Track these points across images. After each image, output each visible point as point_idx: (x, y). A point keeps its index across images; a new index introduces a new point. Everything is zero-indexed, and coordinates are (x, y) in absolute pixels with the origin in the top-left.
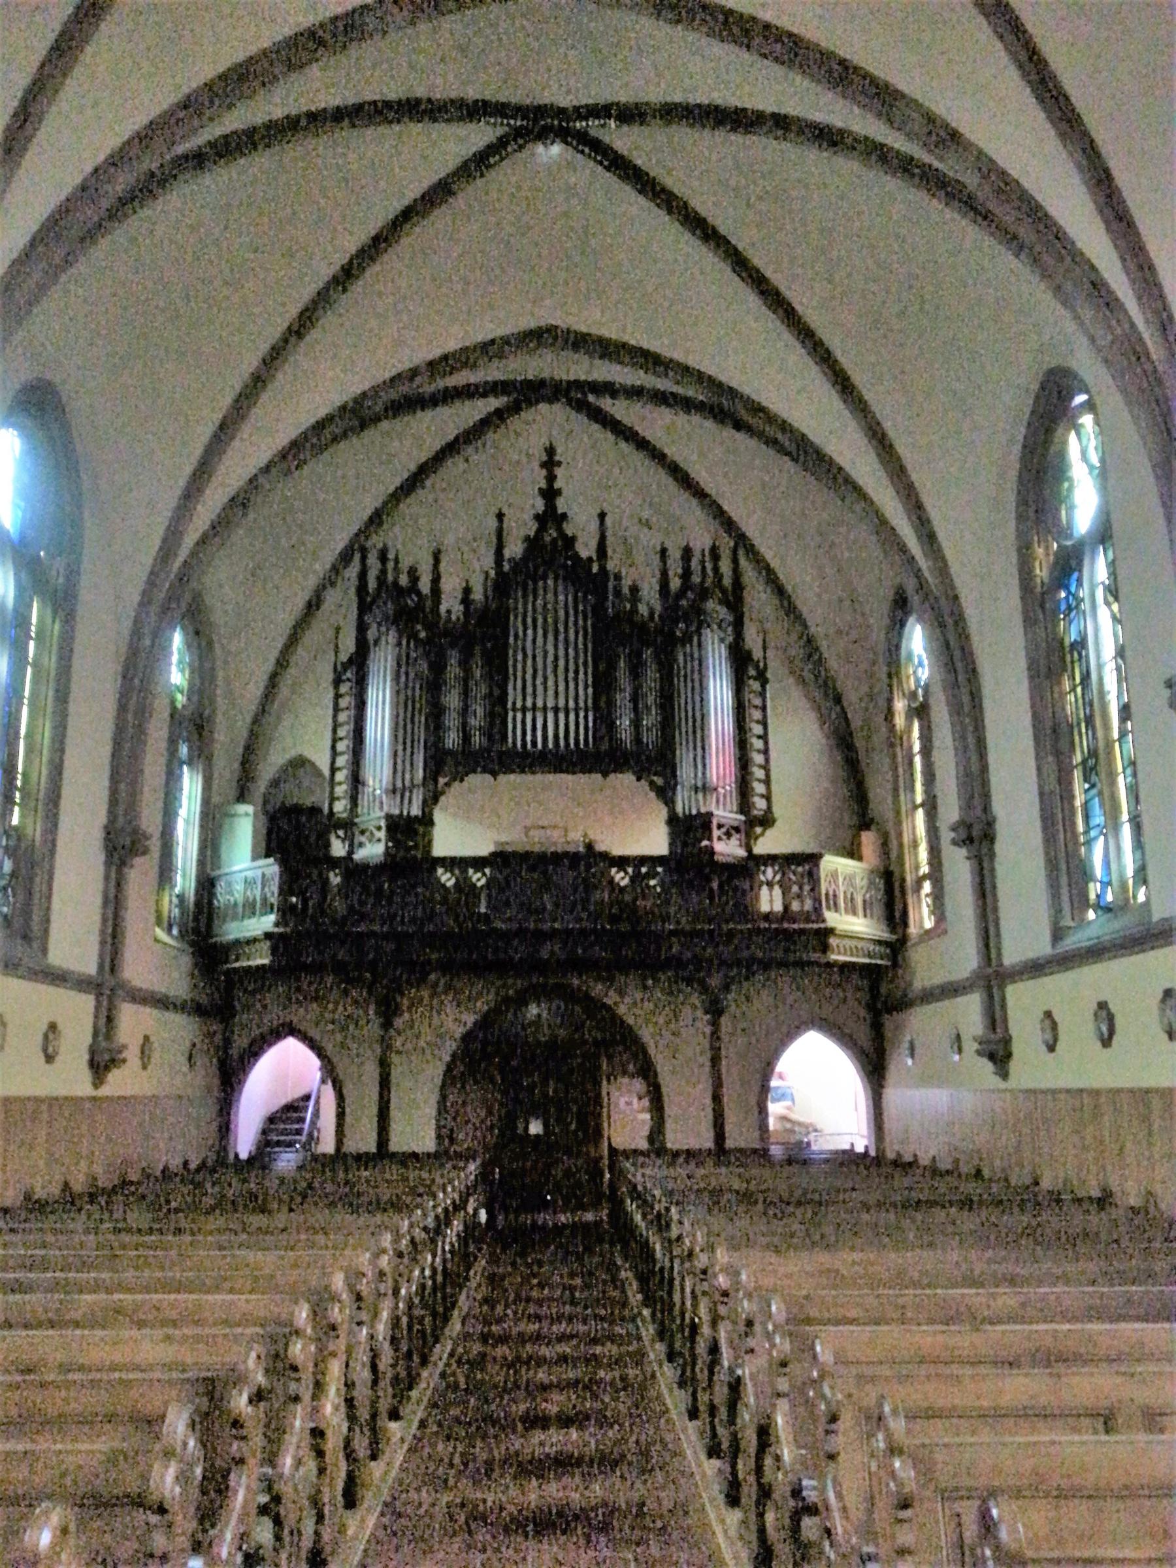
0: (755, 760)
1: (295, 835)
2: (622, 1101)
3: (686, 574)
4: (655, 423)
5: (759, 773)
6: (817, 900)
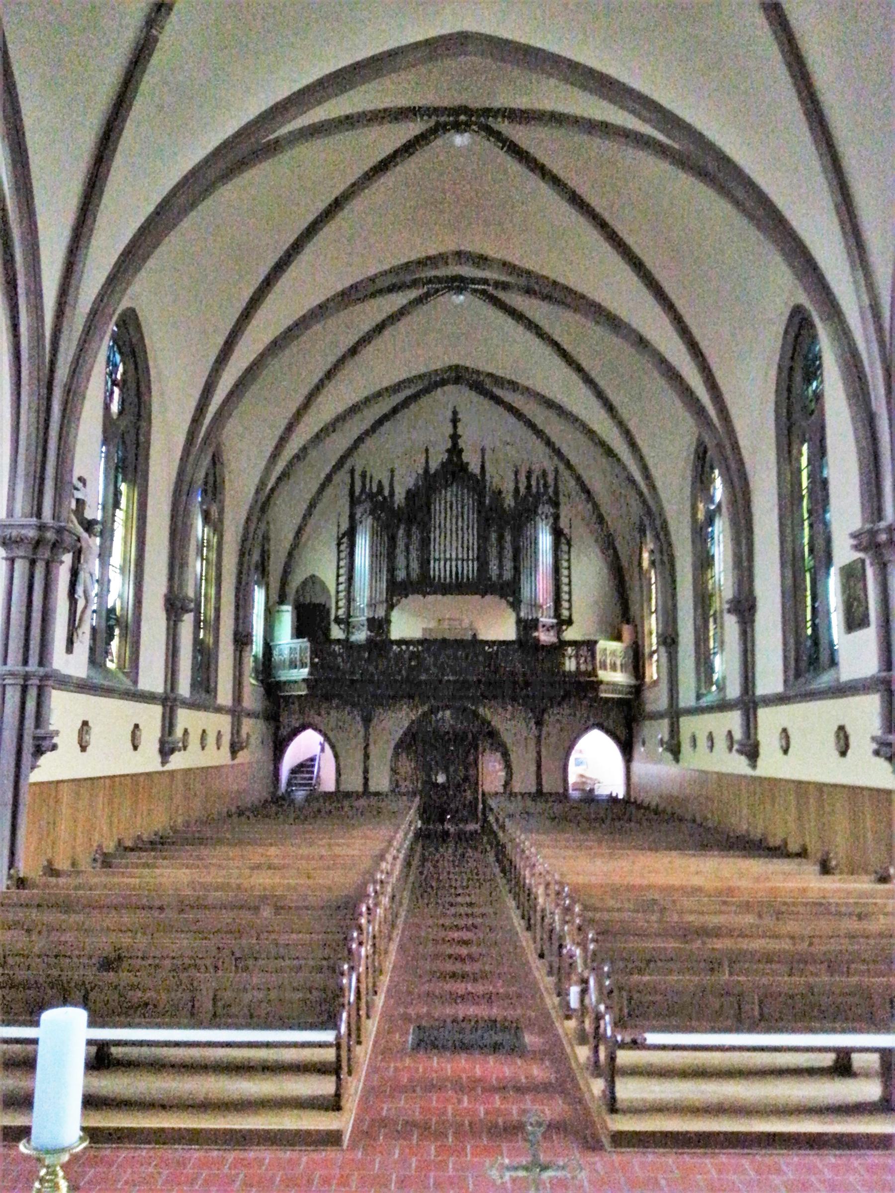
1: (311, 621)
3: (529, 487)
6: (594, 665)
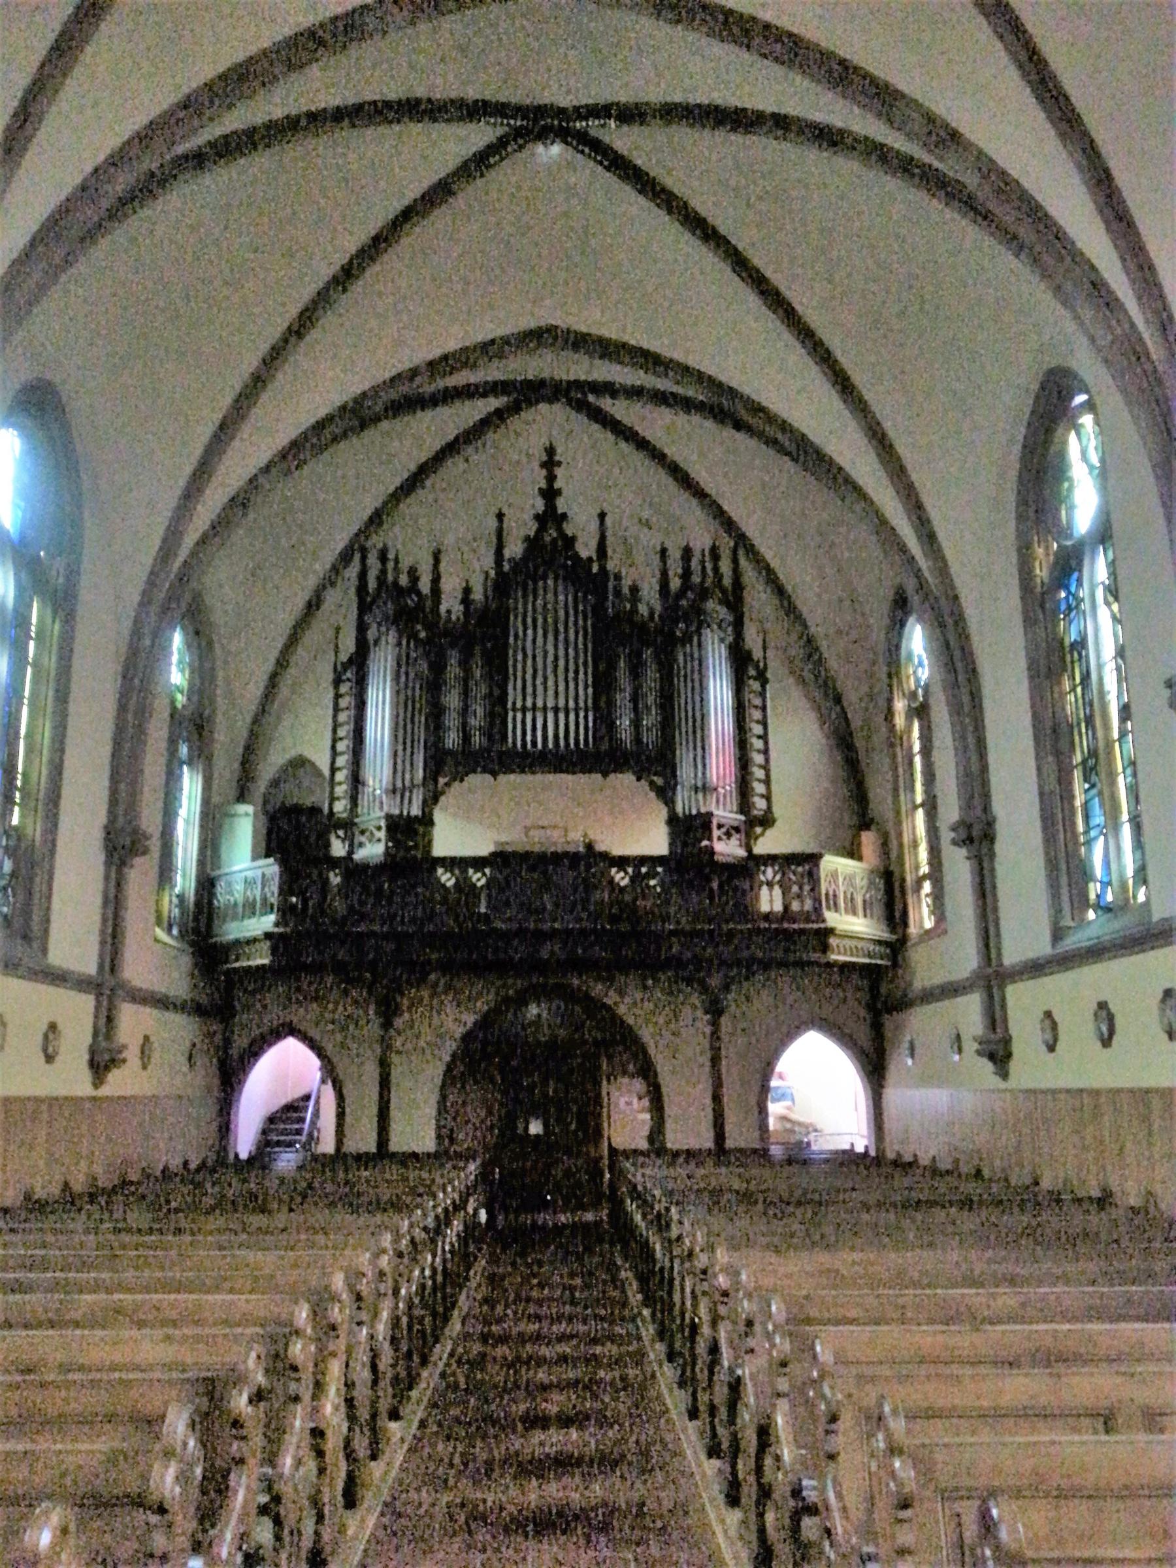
0: (755, 760)
1: (295, 835)
2: (622, 1101)
3: (686, 574)
4: (655, 423)
5: (759, 773)
6: (817, 900)
